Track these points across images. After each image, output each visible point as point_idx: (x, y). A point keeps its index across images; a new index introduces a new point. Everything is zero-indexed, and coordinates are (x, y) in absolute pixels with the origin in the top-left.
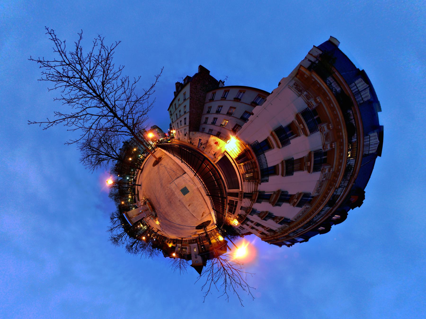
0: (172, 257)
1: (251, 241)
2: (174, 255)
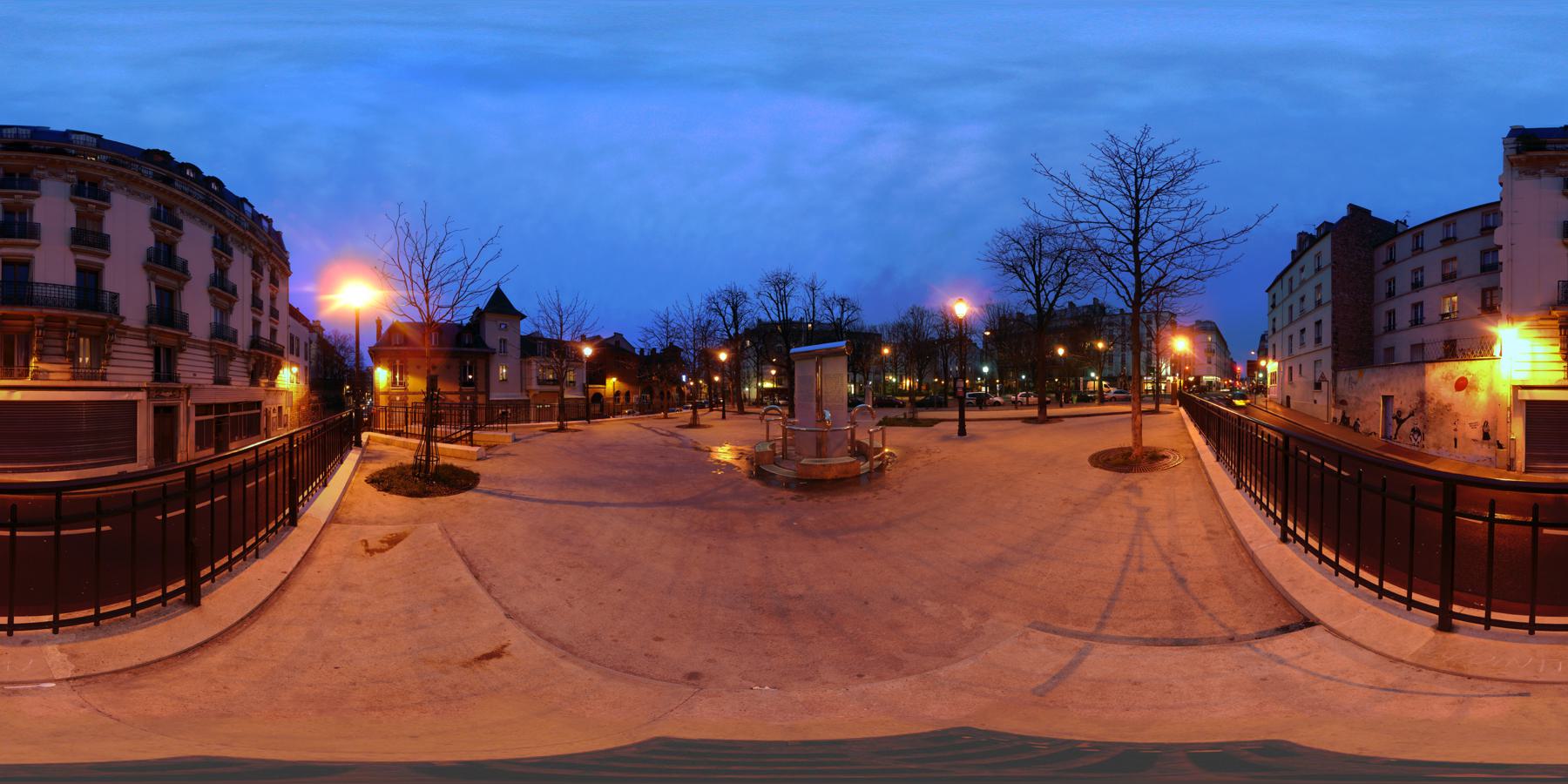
0: (592, 341)
1: (312, 295)
2: (588, 351)
